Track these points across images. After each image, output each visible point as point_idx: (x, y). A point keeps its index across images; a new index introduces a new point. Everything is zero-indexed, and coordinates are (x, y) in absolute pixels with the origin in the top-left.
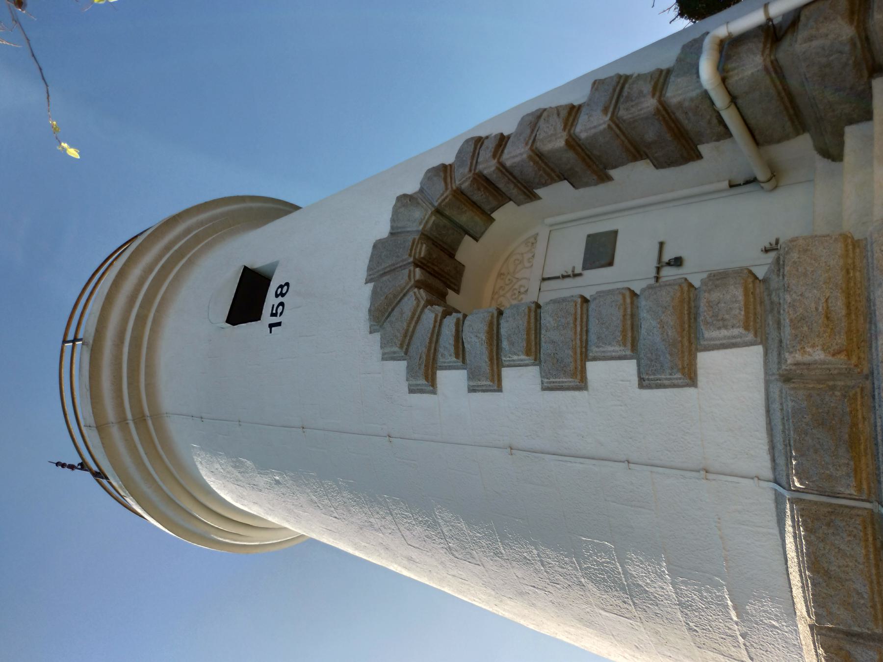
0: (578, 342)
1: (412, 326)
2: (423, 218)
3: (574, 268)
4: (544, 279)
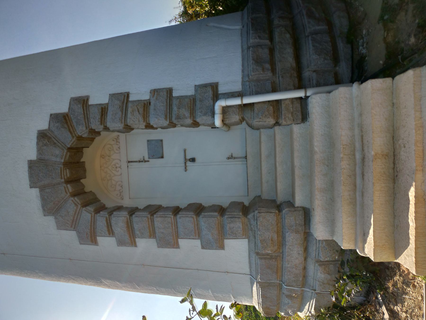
0: (174, 233)
1: (76, 217)
3: (144, 157)
4: (129, 162)
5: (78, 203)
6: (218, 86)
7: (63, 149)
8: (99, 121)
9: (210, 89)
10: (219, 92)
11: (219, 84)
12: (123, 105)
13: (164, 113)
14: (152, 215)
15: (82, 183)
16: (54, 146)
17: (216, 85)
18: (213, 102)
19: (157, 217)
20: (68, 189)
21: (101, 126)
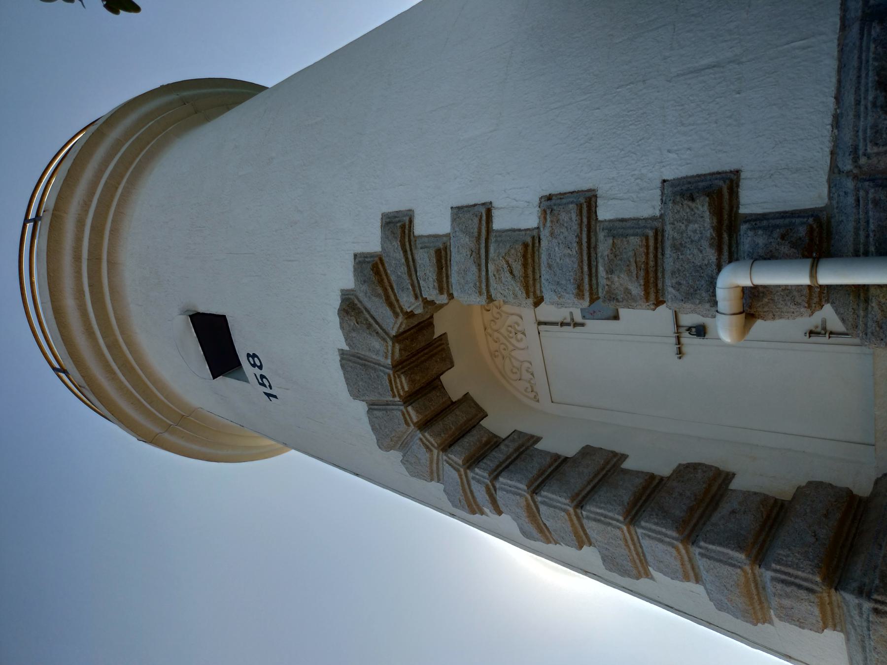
2: (385, 351)
5: (432, 445)
6: (738, 186)
7: (384, 340)
8: (434, 287)
9: (706, 208)
10: (743, 210)
11: (743, 175)
12: (479, 244)
13: (574, 279)
14: (580, 505)
16: (368, 332)
17: (731, 181)
18: (716, 254)
20: (409, 415)
21: (443, 296)
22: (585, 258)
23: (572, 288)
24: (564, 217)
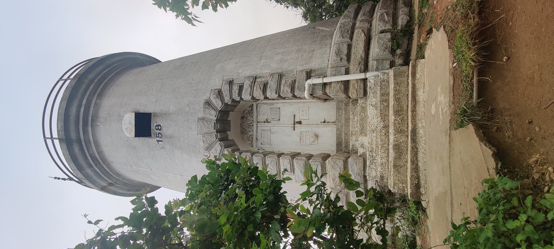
7: (216, 111)
15: (227, 134)
19: (267, 158)
22: (278, 86)
23: (275, 91)
24: (275, 76)
